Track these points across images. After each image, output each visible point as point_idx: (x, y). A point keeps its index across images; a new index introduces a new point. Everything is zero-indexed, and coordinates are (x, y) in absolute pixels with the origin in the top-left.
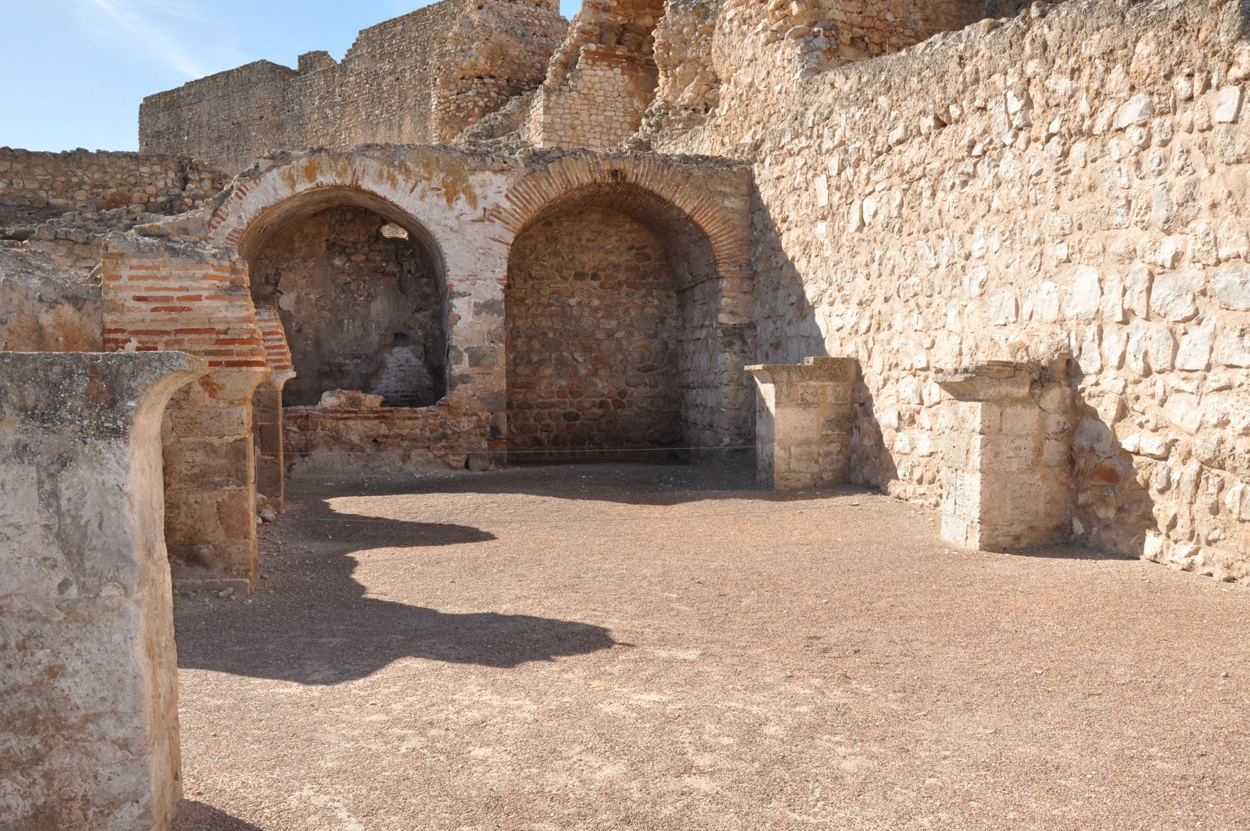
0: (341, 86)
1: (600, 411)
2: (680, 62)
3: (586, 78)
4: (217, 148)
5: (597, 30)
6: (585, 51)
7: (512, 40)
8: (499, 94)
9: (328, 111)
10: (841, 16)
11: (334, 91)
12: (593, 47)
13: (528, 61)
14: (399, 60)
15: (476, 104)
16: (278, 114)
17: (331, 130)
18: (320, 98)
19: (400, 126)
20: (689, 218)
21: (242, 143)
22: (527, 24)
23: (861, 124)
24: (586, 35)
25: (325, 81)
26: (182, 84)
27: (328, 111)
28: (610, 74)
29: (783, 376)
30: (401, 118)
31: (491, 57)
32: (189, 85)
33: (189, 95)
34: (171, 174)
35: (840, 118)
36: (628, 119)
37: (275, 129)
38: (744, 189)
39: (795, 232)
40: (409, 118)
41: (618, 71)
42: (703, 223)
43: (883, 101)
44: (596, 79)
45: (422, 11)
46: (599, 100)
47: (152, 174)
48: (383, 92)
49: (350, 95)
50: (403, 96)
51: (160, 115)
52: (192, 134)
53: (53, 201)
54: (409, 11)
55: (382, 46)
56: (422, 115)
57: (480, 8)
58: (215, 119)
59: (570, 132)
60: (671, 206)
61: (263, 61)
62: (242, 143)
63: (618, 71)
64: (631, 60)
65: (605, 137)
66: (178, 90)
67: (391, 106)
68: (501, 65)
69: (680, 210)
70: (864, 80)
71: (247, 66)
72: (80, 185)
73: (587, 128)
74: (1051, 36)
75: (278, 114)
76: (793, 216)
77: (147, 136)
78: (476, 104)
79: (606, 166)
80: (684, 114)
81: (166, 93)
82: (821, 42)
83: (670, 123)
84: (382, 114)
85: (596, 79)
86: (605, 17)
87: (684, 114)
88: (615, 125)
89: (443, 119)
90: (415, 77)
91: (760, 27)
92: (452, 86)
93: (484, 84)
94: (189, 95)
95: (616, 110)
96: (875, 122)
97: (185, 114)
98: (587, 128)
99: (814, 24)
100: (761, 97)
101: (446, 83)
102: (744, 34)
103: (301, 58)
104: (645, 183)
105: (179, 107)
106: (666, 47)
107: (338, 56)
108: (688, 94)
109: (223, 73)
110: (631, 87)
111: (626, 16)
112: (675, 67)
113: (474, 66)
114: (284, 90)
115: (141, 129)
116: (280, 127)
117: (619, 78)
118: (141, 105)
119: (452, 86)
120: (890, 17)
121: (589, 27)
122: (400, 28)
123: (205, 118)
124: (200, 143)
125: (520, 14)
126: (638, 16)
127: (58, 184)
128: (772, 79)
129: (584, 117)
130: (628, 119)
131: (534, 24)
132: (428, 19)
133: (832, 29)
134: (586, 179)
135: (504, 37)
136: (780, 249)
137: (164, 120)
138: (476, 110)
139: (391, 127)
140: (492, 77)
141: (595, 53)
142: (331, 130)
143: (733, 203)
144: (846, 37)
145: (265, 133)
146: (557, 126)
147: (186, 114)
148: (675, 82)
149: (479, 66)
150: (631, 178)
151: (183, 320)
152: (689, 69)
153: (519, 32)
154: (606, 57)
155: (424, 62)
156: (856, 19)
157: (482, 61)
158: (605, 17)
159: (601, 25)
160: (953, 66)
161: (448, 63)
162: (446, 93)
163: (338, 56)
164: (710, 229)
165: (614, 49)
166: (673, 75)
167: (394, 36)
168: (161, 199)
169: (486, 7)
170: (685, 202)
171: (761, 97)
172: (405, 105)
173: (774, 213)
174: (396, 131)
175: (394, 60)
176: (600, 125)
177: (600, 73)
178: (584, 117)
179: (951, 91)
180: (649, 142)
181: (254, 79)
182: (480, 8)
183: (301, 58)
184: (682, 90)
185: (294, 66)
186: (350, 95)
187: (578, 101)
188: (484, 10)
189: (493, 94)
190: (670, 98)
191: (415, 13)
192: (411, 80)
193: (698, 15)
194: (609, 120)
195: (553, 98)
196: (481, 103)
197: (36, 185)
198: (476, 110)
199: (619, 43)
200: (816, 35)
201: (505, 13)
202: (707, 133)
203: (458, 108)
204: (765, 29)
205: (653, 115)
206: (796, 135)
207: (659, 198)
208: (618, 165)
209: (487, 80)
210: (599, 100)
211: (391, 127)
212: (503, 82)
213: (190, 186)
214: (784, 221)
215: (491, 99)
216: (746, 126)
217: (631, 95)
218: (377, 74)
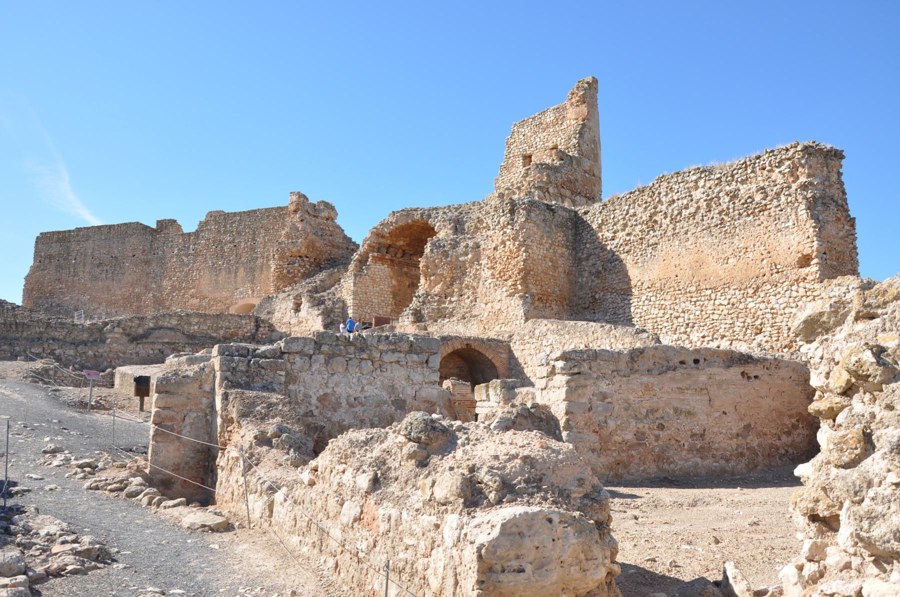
0: (195, 244)
1: (229, 429)
2: (434, 275)
3: (372, 269)
4: (98, 270)
5: (377, 246)
6: (373, 256)
7: (318, 238)
8: (310, 266)
9: (184, 258)
10: (535, 291)
11: (189, 247)
12: (376, 254)
13: (324, 250)
14: (237, 236)
15: (299, 271)
16: (146, 255)
17: (186, 269)
18: (179, 250)
19: (236, 273)
20: (490, 361)
21: (118, 269)
22: (323, 229)
23: (559, 341)
24: (371, 248)
25: (183, 240)
26: (73, 228)
27: (184, 258)
28: (382, 267)
29: (805, 414)
30: (237, 268)
31: (308, 247)
32: (79, 230)
33: (78, 235)
34: (252, 324)
35: (549, 335)
36: (390, 289)
37: (143, 264)
38: (507, 351)
39: (530, 369)
40: (242, 269)
41: (386, 266)
42: (494, 362)
43: (567, 336)
44: (376, 270)
45: (255, 211)
46: (378, 280)
47: (246, 324)
48: (225, 252)
49: (200, 251)
50: (238, 257)
51: (53, 245)
52: (78, 260)
53: (212, 334)
54: (246, 210)
55: (225, 226)
56: (251, 268)
57: (302, 221)
58: (98, 252)
59: (365, 296)
60: (484, 356)
61: (138, 223)
62: (118, 269)
63: (386, 266)
64: (392, 261)
65: (379, 298)
66: (70, 231)
67: (230, 260)
68: (312, 252)
69: (487, 358)
70: (559, 327)
71: (126, 224)
72: (222, 328)
73: (372, 294)
74: (618, 335)
75: (146, 255)
76: (529, 363)
77: (41, 257)
78: (299, 271)
79: (465, 343)
80: (437, 298)
81: (59, 232)
82: (529, 300)
83: (429, 302)
84: (223, 264)
85: (376, 270)
86: (382, 240)
87: (437, 298)
88: (384, 292)
89: (278, 277)
90: (247, 247)
91: (504, 289)
92: (285, 260)
93: (303, 260)
94: (78, 235)
95: (385, 285)
96: (564, 341)
97: (73, 246)
98: (372, 294)
99: (526, 293)
100: (504, 315)
101: (281, 258)
102: (496, 290)
103: (158, 222)
104: (477, 348)
105: (70, 241)
106: (427, 267)
107: (189, 226)
108: (437, 289)
109: (106, 226)
110: (391, 274)
111: (392, 240)
112: (431, 276)
113: (299, 251)
114: (152, 241)
115: (36, 252)
116: (147, 263)
117: (387, 269)
118: (37, 237)
119: (285, 260)
120: (549, 290)
121: (373, 244)
122: (238, 218)
123: (90, 251)
124: (84, 265)
125: (320, 224)
126: (397, 241)
127: (214, 328)
128: (509, 309)
129: (371, 288)
130: (390, 289)
131: (326, 229)
132: (258, 216)
133: (532, 295)
134: (459, 347)
135: (314, 237)
136: (524, 373)
137: (55, 248)
138: (299, 274)
139: (229, 272)
140: (307, 257)
141: (377, 257)
142: (186, 269)
143: (504, 356)
144: (536, 298)
145: (136, 265)
146: (359, 293)
147: (73, 246)
148: (430, 283)
149: (302, 252)
150: (473, 347)
151: (466, 398)
152: (438, 278)
153: (320, 234)
154: (381, 259)
155: (254, 239)
156: (539, 292)
157: (303, 249)
158: (382, 240)
159: (379, 244)
160: (591, 333)
161: (284, 248)
162: (281, 263)
163: (189, 226)
164: (497, 364)
165: (385, 256)
166: (430, 280)
167: (234, 222)
168: (249, 334)
169: (305, 221)
170: (489, 355)
171: (504, 315)
172: (240, 261)
173: (521, 361)
174: (233, 275)
175: (233, 236)
176: (378, 292)
177: (378, 267)
178: (371, 288)
179: (590, 339)
180: (420, 310)
181: (130, 232)
182: (302, 221)
183: (158, 222)
184: (434, 287)
185: (154, 226)
186: (200, 251)
187: (368, 281)
188: (305, 222)
189: (307, 266)
190: (428, 290)
191: (249, 212)
192: (244, 248)
193: (444, 255)
194: (382, 290)
195: (358, 279)
196: (302, 271)
197: (206, 328)
198: (299, 274)
199: (387, 253)
200: (527, 297)
201: (313, 223)
202: (475, 322)
203: (288, 272)
204: (506, 291)
205: (420, 297)
206: (531, 337)
207: (480, 353)
208: (469, 342)
209: (305, 259)
210: (378, 280)
211: (229, 272)
212: (312, 260)
213: (261, 329)
214: (525, 364)
215: (307, 269)
216: (497, 323)
217: (392, 278)
218: (220, 241)
